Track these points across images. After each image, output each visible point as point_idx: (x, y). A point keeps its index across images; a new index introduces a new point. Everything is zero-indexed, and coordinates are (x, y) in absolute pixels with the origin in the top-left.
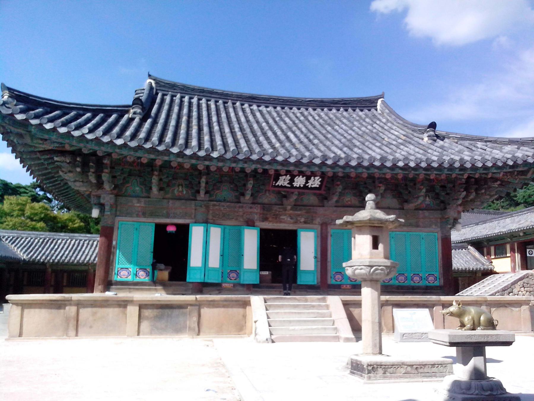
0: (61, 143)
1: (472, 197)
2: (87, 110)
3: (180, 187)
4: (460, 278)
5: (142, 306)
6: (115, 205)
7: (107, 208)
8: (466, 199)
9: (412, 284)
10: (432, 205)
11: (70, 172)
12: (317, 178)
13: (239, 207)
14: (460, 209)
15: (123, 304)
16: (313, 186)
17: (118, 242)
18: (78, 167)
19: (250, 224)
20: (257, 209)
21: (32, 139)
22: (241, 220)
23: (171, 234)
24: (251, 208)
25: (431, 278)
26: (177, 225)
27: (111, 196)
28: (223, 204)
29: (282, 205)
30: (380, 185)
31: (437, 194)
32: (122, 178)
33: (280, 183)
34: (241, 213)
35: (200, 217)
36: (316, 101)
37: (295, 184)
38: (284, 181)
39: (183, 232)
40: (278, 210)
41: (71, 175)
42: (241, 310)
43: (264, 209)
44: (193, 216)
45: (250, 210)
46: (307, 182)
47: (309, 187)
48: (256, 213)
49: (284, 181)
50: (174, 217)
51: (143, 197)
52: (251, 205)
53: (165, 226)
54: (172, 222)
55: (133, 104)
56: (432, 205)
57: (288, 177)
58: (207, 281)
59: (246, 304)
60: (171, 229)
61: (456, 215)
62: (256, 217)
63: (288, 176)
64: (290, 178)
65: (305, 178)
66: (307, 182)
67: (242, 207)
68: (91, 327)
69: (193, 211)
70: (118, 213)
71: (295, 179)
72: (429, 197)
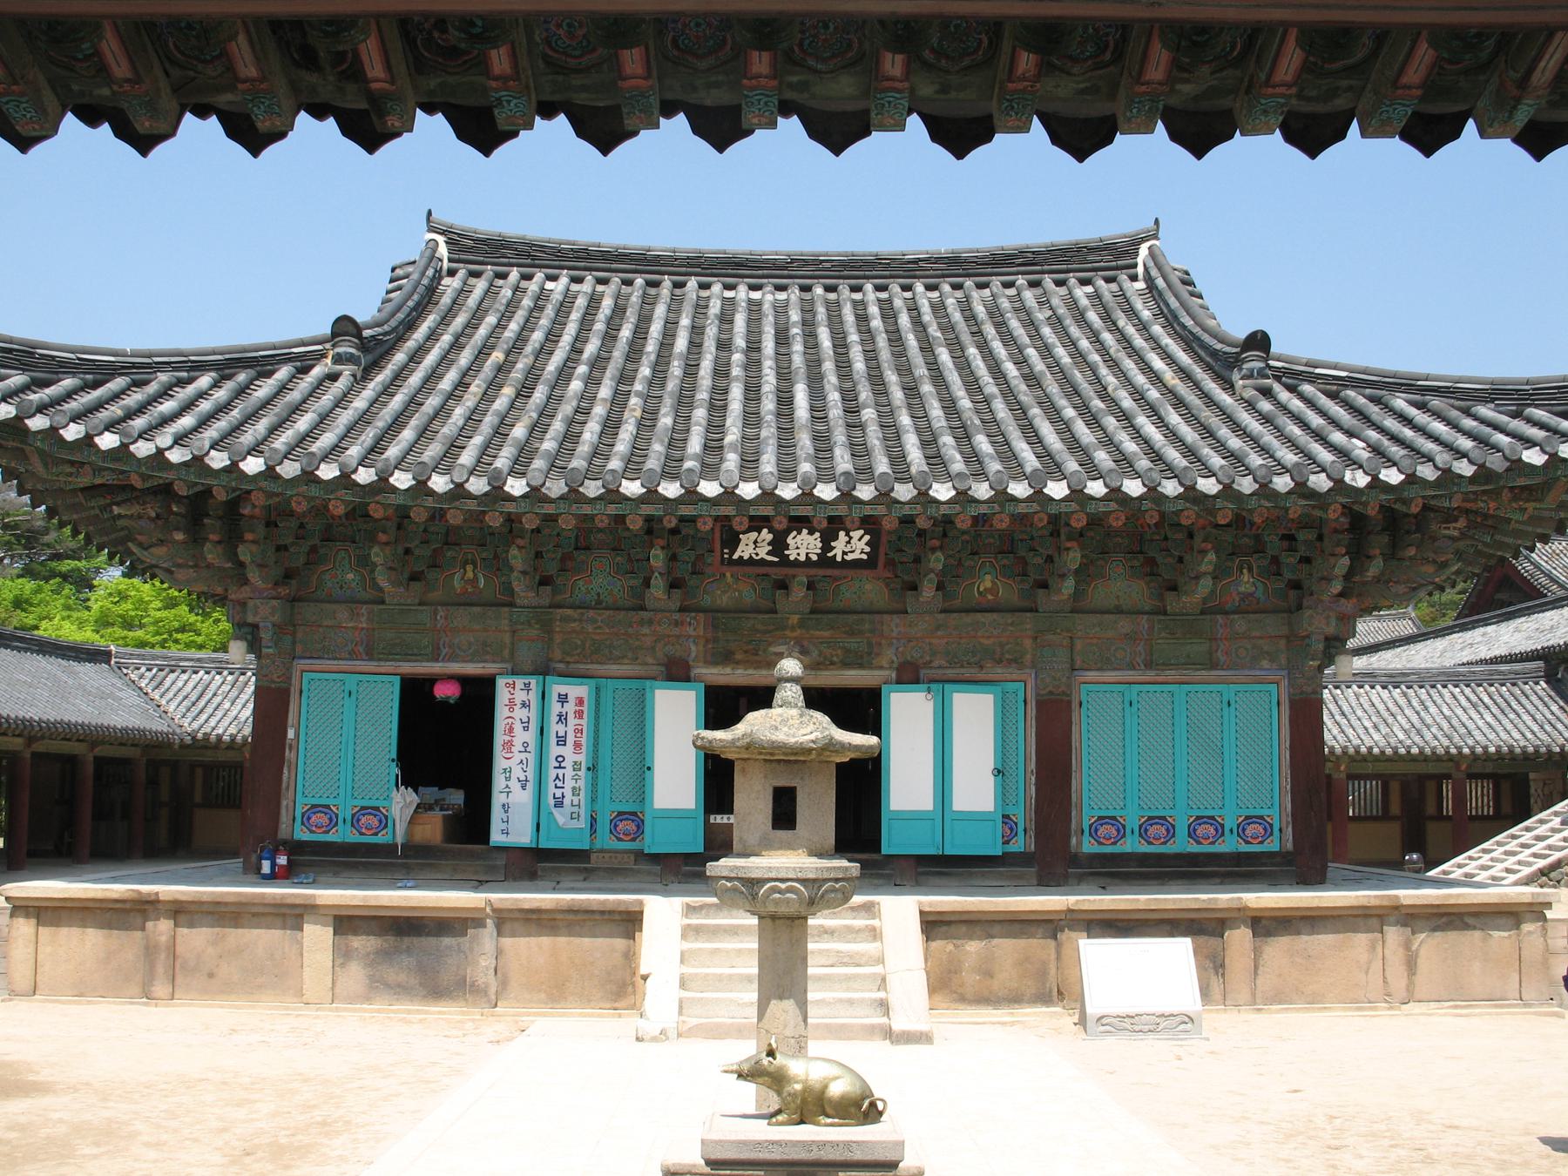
0: (123, 472)
1: (1374, 568)
2: (200, 367)
3: (469, 568)
4: (1532, 776)
5: (346, 923)
6: (285, 628)
7: (266, 635)
8: (1357, 578)
10: (1259, 594)
11: (161, 542)
12: (856, 534)
13: (642, 623)
14: (1347, 605)
15: (292, 916)
16: (849, 557)
18: (177, 529)
19: (677, 673)
20: (695, 627)
21: (46, 465)
23: (444, 703)
24: (676, 624)
26: (465, 681)
27: (275, 602)
28: (591, 613)
30: (1068, 545)
31: (1275, 560)
32: (305, 549)
33: (745, 550)
35: (526, 654)
36: (938, 260)
39: (480, 695)
40: (760, 627)
41: (160, 551)
42: (620, 943)
43: (715, 627)
44: (506, 653)
45: (676, 631)
46: (827, 547)
47: (839, 559)
50: (452, 658)
51: (366, 603)
52: (677, 616)
53: (431, 681)
54: (448, 670)
55: (334, 334)
56: (1259, 594)
57: (766, 535)
58: (544, 844)
59: (630, 922)
60: (446, 692)
61: (1331, 630)
63: (765, 531)
64: (770, 537)
65: (817, 535)
66: (827, 547)
67: (650, 622)
68: (211, 975)
69: (507, 638)
70: (299, 649)
71: (789, 540)
72: (1250, 570)
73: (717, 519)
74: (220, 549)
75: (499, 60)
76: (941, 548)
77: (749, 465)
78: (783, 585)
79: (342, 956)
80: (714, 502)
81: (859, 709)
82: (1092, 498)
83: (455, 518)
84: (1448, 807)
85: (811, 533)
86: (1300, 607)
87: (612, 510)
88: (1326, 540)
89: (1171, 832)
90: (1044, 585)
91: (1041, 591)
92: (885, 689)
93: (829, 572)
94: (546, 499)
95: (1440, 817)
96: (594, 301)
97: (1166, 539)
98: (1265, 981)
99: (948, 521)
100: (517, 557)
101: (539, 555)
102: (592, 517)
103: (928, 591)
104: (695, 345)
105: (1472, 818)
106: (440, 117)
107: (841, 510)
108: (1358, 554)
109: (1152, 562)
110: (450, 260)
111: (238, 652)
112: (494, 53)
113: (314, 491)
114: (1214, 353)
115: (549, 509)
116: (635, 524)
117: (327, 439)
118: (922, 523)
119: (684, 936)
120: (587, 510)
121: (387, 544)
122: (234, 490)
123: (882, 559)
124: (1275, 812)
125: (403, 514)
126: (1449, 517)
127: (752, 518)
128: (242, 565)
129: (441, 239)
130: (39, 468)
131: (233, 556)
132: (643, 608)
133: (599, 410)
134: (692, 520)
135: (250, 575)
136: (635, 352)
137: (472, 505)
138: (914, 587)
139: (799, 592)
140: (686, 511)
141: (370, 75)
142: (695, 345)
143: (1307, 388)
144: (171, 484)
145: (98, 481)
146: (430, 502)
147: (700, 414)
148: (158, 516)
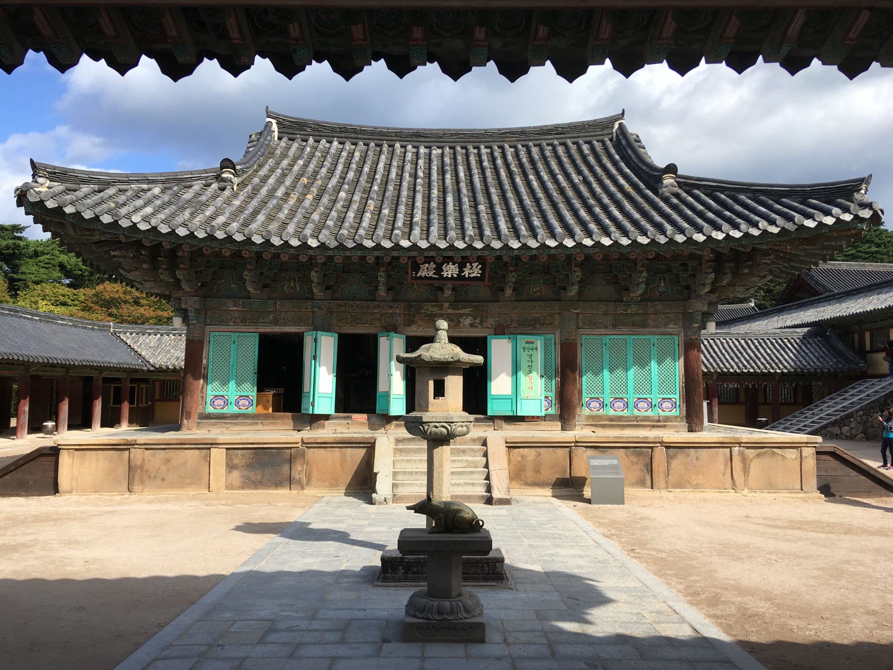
0: (115, 234)
7: (191, 314)
9: (636, 413)
11: (136, 269)
12: (475, 265)
13: (374, 307)
14: (713, 298)
16: (472, 275)
17: (211, 360)
20: (399, 309)
21: (75, 230)
22: (378, 324)
24: (391, 307)
25: (667, 405)
29: (437, 301)
33: (423, 273)
34: (378, 315)
37: (445, 274)
38: (427, 271)
44: (310, 322)
46: (461, 271)
48: (400, 315)
49: (427, 271)
50: (285, 325)
61: (705, 308)
62: (400, 320)
66: (461, 271)
67: (379, 307)
68: (163, 479)
69: (310, 315)
70: (208, 321)
72: (665, 281)
73: (410, 258)
74: (167, 273)
75: (294, 30)
76: (515, 271)
77: (427, 233)
78: (441, 289)
79: (230, 467)
80: (409, 249)
81: (477, 345)
82: (586, 246)
83: (284, 258)
84: (770, 399)
85: (454, 264)
86: (689, 298)
87: (359, 253)
88: (703, 265)
89: (626, 405)
90: (564, 288)
91: (562, 292)
92: (489, 338)
93: (462, 283)
94: (328, 248)
95: (766, 403)
96: (351, 155)
97: (623, 266)
98: (672, 478)
99: (518, 258)
100: (382, 277)
101: (325, 275)
102: (350, 257)
103: (509, 292)
104: (401, 176)
105: (781, 404)
106: (267, 59)
107: (468, 253)
108: (719, 272)
109: (616, 277)
110: (279, 132)
111: (177, 322)
112: (291, 26)
113: (214, 244)
114: (649, 176)
115: (330, 253)
116: (371, 260)
117: (221, 219)
118: (505, 259)
119: (395, 453)
120: (348, 253)
121: (251, 270)
122: (173, 243)
123: (487, 276)
124: (677, 396)
125: (259, 255)
126: (766, 254)
127: (426, 257)
128: (179, 280)
129: (274, 121)
130: (72, 232)
131: (174, 276)
132: (375, 300)
133: (355, 207)
134: (397, 258)
135: (183, 286)
136: (372, 180)
137: (293, 251)
138: (503, 290)
139: (448, 293)
140: (395, 254)
141: (232, 36)
142: (401, 176)
143: (697, 192)
144: (141, 240)
145: (103, 239)
146: (272, 250)
147: (402, 208)
148: (134, 257)
